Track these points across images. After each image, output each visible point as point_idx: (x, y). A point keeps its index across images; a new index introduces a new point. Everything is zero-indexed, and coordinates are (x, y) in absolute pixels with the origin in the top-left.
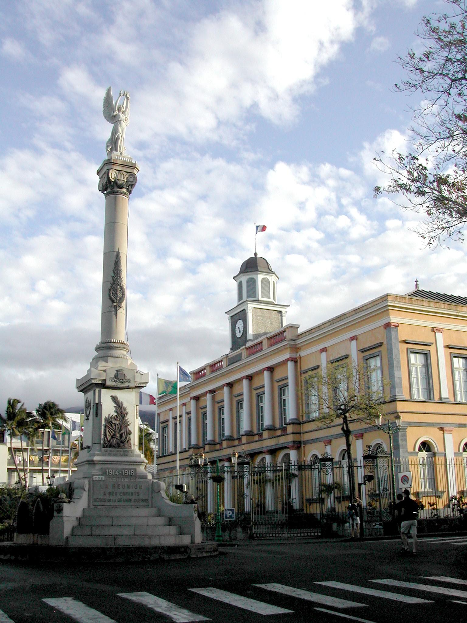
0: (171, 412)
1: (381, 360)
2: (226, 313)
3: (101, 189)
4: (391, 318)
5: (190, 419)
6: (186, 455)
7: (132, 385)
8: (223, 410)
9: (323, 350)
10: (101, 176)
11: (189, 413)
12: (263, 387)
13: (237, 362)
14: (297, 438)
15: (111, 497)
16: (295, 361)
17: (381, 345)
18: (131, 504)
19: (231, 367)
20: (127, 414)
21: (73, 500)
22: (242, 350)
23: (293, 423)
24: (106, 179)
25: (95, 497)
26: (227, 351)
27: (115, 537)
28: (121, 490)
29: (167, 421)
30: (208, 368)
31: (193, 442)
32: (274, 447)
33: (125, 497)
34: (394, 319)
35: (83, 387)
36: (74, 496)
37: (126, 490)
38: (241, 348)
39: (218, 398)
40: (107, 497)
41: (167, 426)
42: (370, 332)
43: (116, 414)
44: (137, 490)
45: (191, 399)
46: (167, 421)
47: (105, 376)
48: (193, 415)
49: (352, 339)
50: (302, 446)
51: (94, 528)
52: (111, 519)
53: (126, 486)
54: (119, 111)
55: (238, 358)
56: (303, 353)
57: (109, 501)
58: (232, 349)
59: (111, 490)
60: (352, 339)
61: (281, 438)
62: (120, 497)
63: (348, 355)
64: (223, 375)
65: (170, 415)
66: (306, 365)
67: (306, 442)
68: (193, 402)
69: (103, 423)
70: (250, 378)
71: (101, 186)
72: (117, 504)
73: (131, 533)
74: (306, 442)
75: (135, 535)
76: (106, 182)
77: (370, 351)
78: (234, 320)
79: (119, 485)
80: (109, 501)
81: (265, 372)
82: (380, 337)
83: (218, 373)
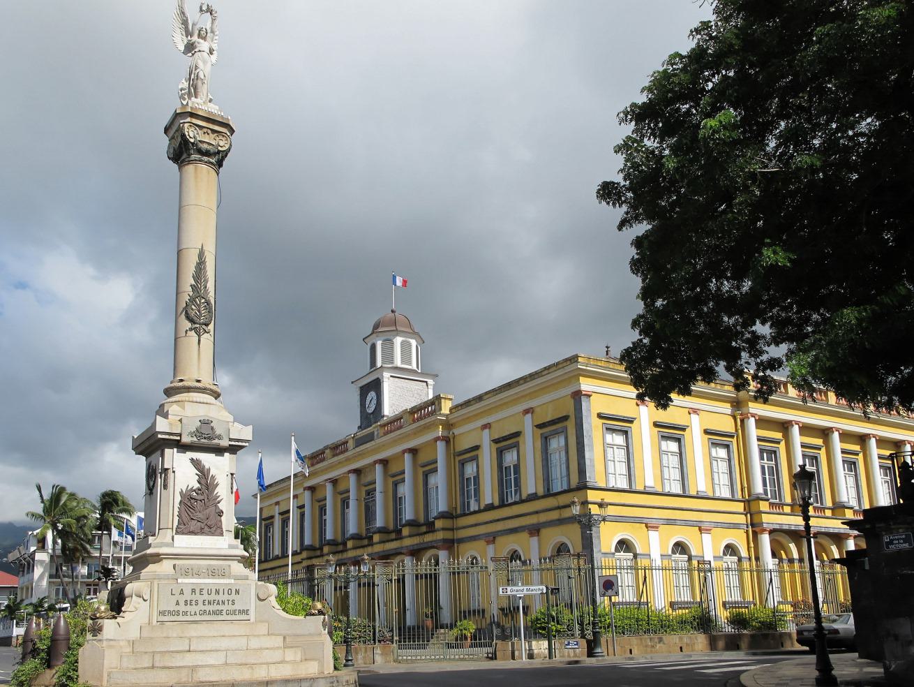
0: (277, 506)
1: (566, 438)
2: (352, 382)
3: (172, 156)
4: (582, 385)
5: (302, 515)
6: (298, 558)
7: (225, 443)
8: (348, 504)
9: (485, 427)
10: (171, 135)
11: (301, 507)
12: (403, 472)
13: (368, 442)
14: (449, 535)
15: (188, 608)
16: (447, 440)
17: (566, 418)
18: (220, 618)
19: (358, 449)
20: (217, 485)
21: (122, 614)
22: (374, 428)
23: (443, 516)
24: (179, 139)
25: (161, 609)
26: (355, 429)
27: (194, 668)
28: (206, 597)
29: (272, 517)
30: (328, 451)
31: (307, 542)
32: (416, 547)
33: (211, 608)
34: (586, 385)
35: (143, 447)
36: (123, 609)
37: (213, 597)
38: (373, 426)
39: (341, 487)
40: (182, 608)
41: (272, 524)
42: (549, 403)
43: (198, 485)
44: (231, 598)
45: (304, 490)
46: (272, 517)
47: (180, 428)
48: (307, 510)
49: (526, 412)
50: (456, 545)
51: (157, 657)
52: (188, 641)
53: (214, 591)
54: (199, 36)
55: (370, 438)
56: (456, 431)
57: (185, 613)
58: (359, 427)
59: (188, 595)
60: (526, 412)
61: (427, 536)
62: (203, 608)
63: (521, 432)
64: (348, 460)
65: (277, 510)
66: (464, 444)
67: (461, 541)
68: (307, 494)
69: (178, 499)
70: (385, 462)
71: (172, 151)
72: (198, 618)
73: (222, 661)
74: (461, 541)
75: (226, 664)
76: (180, 144)
77: (550, 427)
78: (364, 391)
79: (201, 590)
80: (185, 613)
81: (406, 455)
82: (569, 409)
83: (341, 457)
